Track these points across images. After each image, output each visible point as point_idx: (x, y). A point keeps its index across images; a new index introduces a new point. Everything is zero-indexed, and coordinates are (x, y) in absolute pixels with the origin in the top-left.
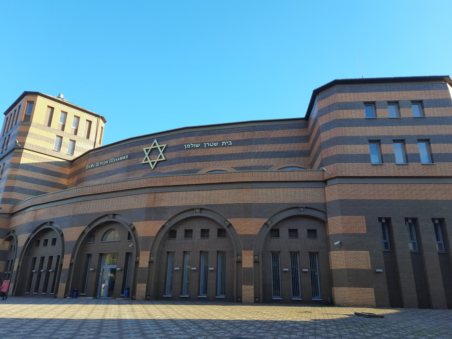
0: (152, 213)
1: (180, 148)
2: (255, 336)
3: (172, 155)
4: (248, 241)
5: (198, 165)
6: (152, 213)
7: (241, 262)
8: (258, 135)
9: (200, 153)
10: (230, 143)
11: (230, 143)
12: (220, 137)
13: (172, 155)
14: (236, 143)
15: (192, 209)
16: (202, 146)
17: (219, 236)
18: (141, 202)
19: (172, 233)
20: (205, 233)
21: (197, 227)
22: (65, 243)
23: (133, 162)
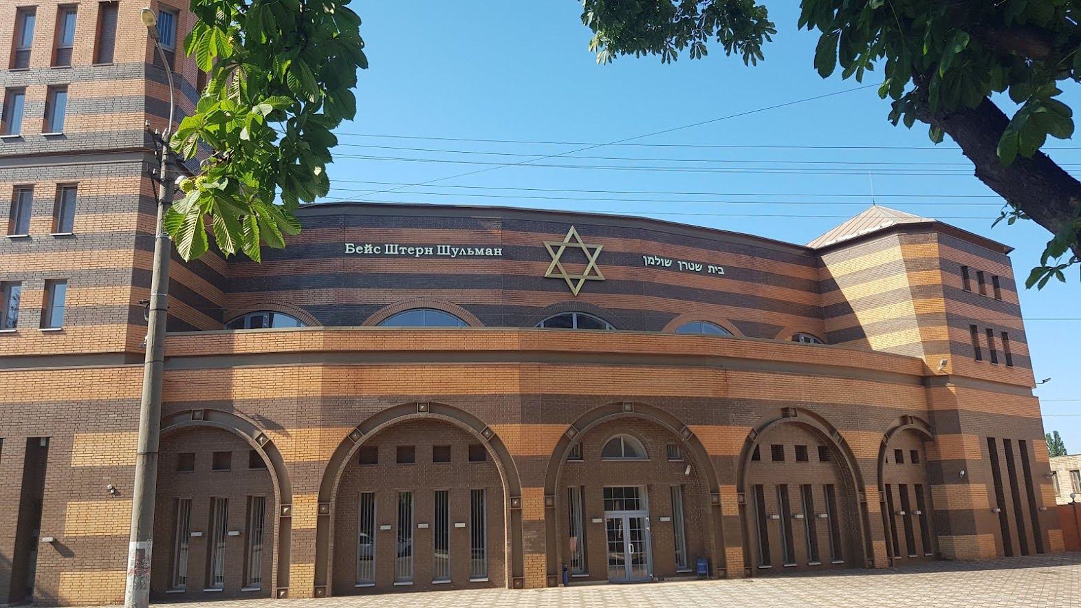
0: (537, 408)
1: (635, 260)
2: (950, 605)
3: (619, 273)
4: (529, 470)
5: (672, 304)
6: (537, 408)
7: (520, 511)
8: (761, 264)
9: (672, 279)
10: (720, 270)
11: (720, 270)
12: (703, 254)
13: (619, 273)
14: (731, 273)
15: (413, 405)
16: (675, 266)
17: (412, 460)
18: (504, 382)
19: (368, 456)
20: (442, 454)
21: (424, 447)
22: (876, 482)
23: (517, 267)
